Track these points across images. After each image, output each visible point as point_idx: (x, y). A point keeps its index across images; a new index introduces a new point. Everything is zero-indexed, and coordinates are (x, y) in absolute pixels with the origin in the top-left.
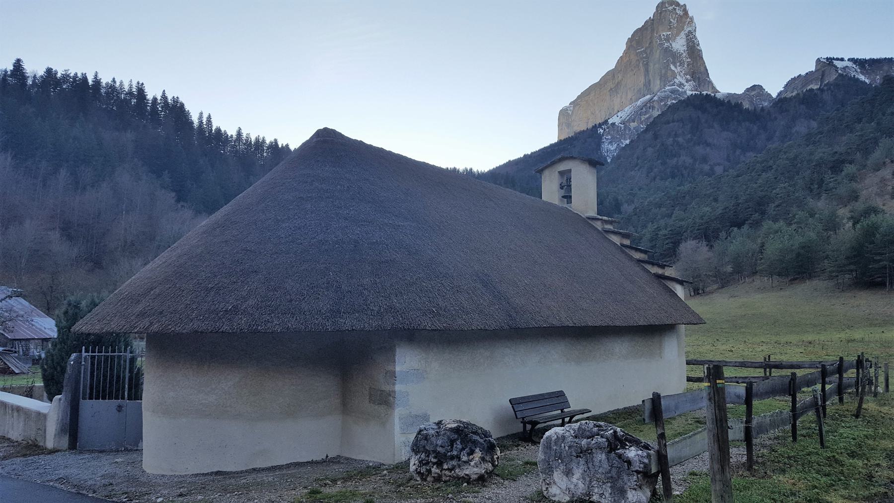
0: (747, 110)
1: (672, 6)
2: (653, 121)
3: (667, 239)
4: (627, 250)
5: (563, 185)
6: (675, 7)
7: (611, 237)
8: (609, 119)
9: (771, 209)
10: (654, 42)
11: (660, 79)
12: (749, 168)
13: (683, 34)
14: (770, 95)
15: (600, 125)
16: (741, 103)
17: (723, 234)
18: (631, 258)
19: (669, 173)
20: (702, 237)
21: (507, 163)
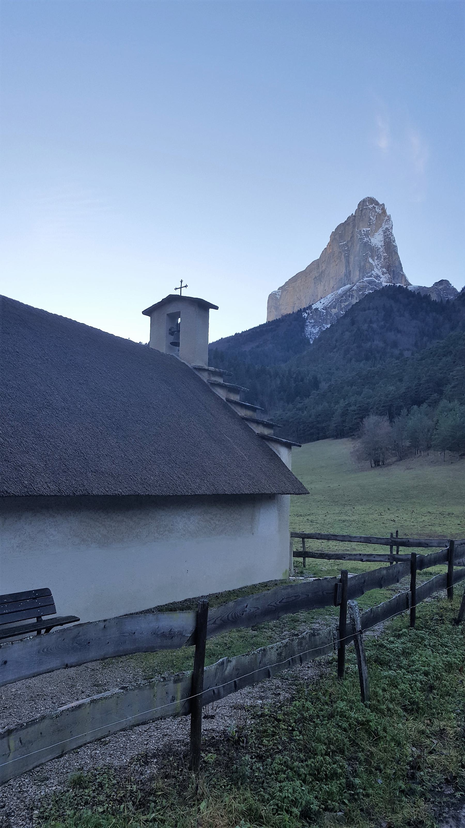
0: (435, 302)
1: (372, 204)
2: (351, 308)
3: (356, 414)
4: (233, 407)
5: (173, 330)
6: (375, 206)
7: (217, 391)
8: (313, 304)
9: (448, 389)
10: (355, 237)
11: (359, 271)
12: (431, 353)
13: (380, 231)
14: (454, 289)
15: (305, 310)
16: (430, 294)
17: (404, 411)
18: (234, 415)
19: (363, 356)
20: (387, 413)
21: (220, 340)
